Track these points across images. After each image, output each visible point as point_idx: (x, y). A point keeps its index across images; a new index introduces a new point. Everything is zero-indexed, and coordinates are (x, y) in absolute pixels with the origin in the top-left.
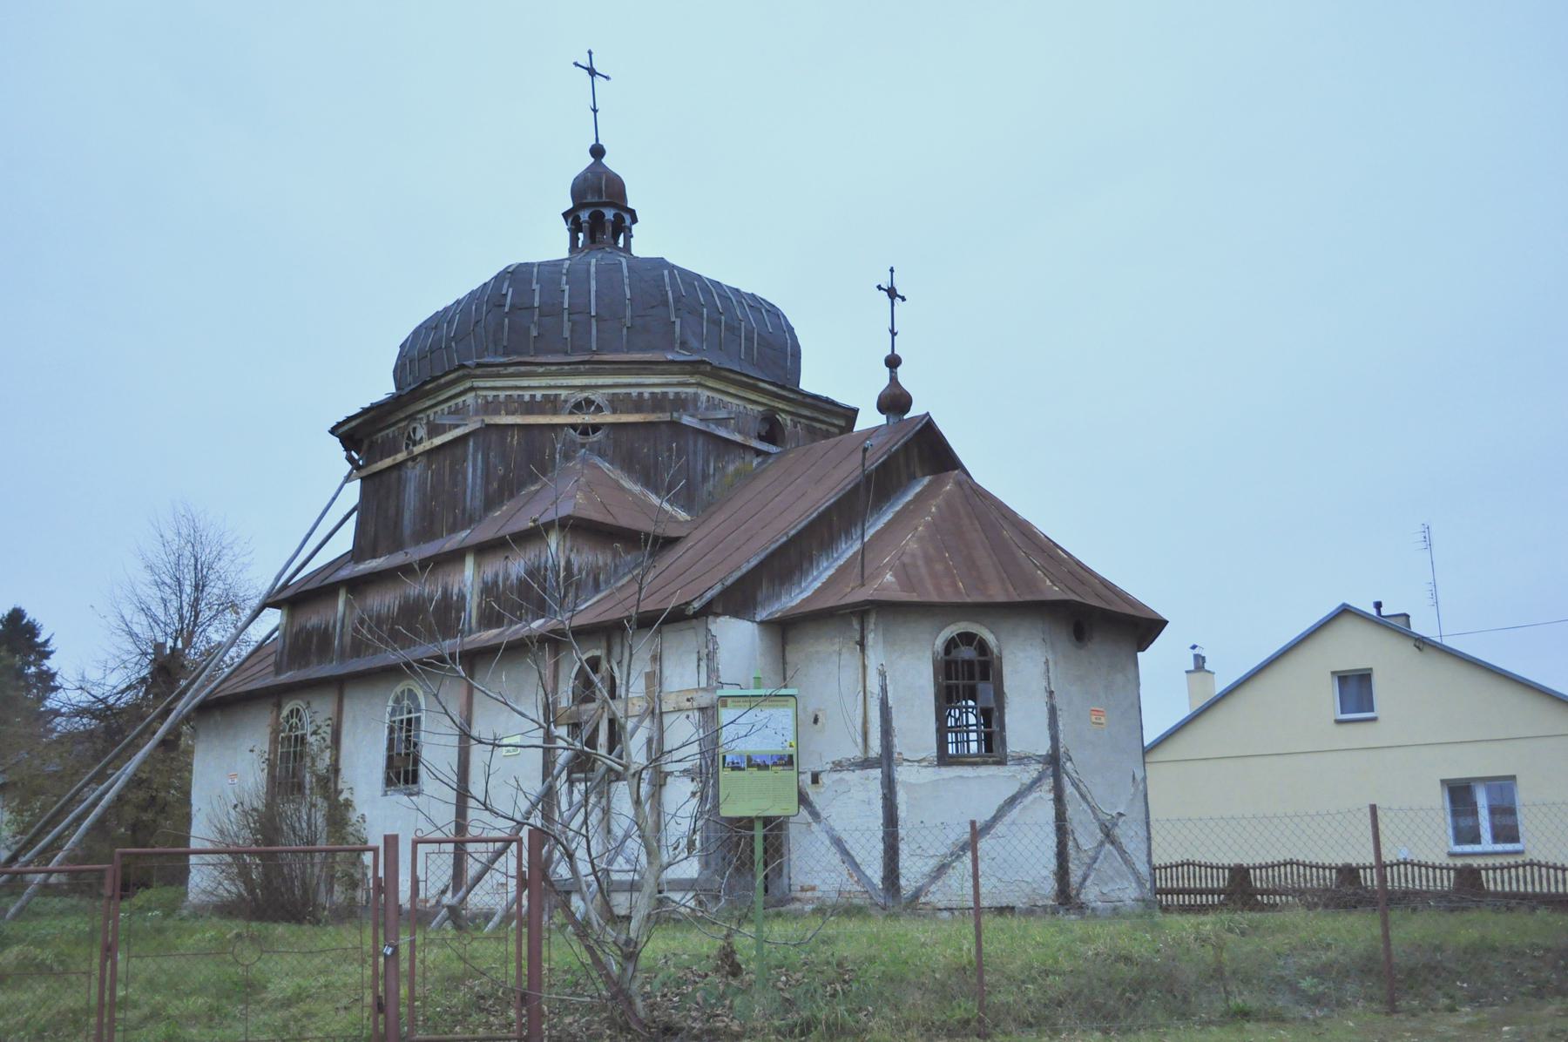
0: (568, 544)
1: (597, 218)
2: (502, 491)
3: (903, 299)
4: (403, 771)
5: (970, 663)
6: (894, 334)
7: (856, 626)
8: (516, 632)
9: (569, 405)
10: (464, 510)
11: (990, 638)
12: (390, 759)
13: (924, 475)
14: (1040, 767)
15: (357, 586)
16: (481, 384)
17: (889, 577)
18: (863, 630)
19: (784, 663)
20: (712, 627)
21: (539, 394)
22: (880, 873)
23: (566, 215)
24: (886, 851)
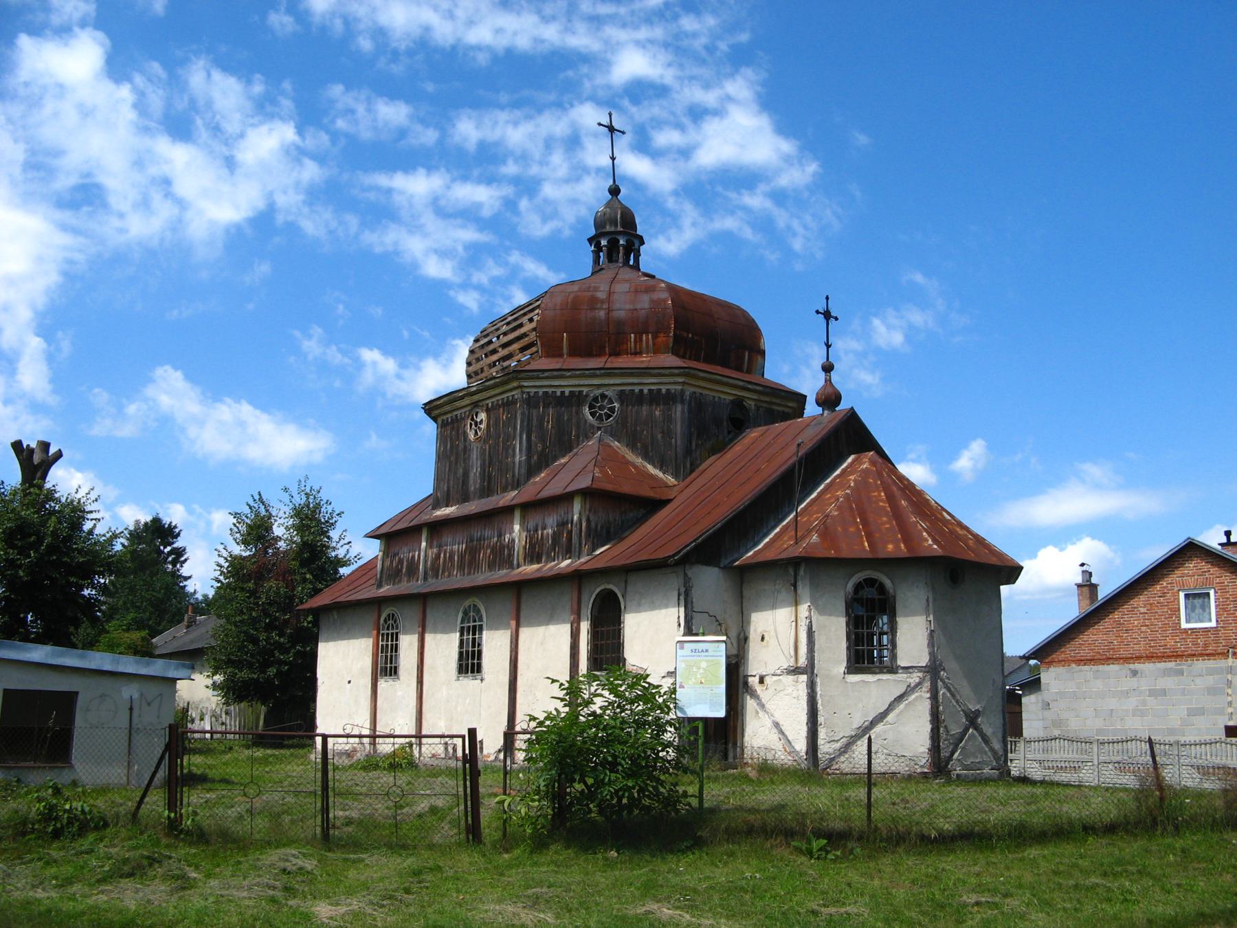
1: (613, 244)
5: (873, 600)
7: (791, 572)
9: (590, 399)
11: (888, 583)
12: (461, 654)
14: (920, 675)
15: (437, 528)
17: (815, 538)
19: (742, 593)
20: (689, 573)
21: (567, 391)
23: (590, 240)
24: (932, 730)
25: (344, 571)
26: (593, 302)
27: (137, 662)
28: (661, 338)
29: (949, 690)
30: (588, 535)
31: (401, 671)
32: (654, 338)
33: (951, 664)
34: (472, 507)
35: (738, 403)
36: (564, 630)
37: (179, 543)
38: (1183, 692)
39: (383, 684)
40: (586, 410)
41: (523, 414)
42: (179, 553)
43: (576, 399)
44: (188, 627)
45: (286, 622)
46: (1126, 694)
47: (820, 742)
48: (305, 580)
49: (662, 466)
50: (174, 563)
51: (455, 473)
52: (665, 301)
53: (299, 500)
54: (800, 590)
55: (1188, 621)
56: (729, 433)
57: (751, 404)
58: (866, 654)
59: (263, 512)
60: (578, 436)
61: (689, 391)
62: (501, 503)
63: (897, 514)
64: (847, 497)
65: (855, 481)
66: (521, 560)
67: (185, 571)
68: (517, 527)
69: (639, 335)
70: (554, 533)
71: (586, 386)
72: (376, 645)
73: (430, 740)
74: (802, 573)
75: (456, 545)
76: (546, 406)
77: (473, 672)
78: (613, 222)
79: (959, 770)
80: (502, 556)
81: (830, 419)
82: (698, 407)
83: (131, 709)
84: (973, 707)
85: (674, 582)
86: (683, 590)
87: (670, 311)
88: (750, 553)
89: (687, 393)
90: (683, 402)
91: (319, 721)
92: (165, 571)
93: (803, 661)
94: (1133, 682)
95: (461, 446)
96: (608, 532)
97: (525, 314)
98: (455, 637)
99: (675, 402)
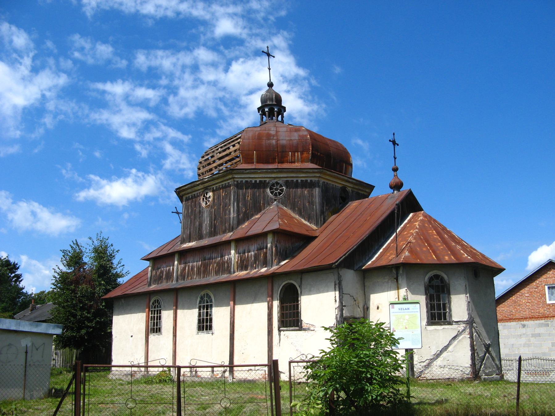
0: (276, 239)
3: (398, 145)
5: (438, 286)
6: (395, 158)
9: (270, 185)
10: (230, 224)
11: (445, 277)
12: (199, 320)
14: (464, 325)
15: (183, 254)
16: (236, 176)
17: (407, 253)
18: (397, 274)
19: (364, 283)
20: (341, 273)
21: (258, 180)
24: (472, 354)
25: (120, 280)
26: (269, 136)
27: (31, 325)
28: (305, 155)
29: (477, 333)
30: (276, 254)
31: (163, 330)
32: (302, 154)
33: (477, 320)
34: (205, 242)
35: (344, 189)
36: (263, 306)
37: (18, 272)
38: (549, 335)
39: (152, 337)
40: (268, 190)
41: (234, 192)
42: (18, 277)
43: (262, 185)
44: (32, 310)
45: (91, 306)
46: (520, 336)
47: (415, 363)
48: (100, 284)
49: (309, 219)
50: (16, 281)
51: (194, 225)
52: (306, 136)
53: (97, 243)
54: (400, 282)
55: (550, 300)
56: (340, 204)
57: (349, 189)
58: (438, 315)
59: (78, 250)
60: (264, 204)
61: (322, 181)
63: (444, 242)
64: (417, 233)
65: (419, 225)
66: (236, 269)
67: (21, 285)
68: (233, 252)
69: (294, 152)
70: (255, 254)
71: (267, 177)
72: (148, 316)
73: (240, 368)
74: (401, 272)
75: (196, 264)
76: (247, 188)
77: (206, 329)
78: (271, 100)
79: (484, 376)
80: (224, 267)
81: (398, 196)
82: (326, 190)
83: (26, 352)
84: (488, 342)
85: (332, 278)
86: (337, 282)
87: (309, 141)
88: (370, 263)
89: (321, 182)
90: (319, 187)
91: (114, 357)
92: (11, 285)
94: (523, 331)
95: (198, 210)
96: (286, 253)
97: (229, 143)
98: (196, 311)
99: (315, 187)
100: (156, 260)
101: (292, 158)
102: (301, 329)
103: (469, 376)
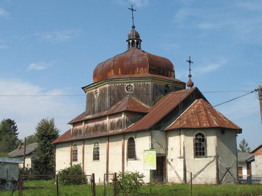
1: (133, 42)
2: (113, 103)
3: (192, 63)
4: (96, 157)
8: (117, 132)
11: (204, 134)
12: (94, 155)
13: (196, 99)
17: (185, 122)
19: (167, 137)
22: (183, 178)
23: (127, 41)
24: (217, 173)
34: (96, 115)
35: (167, 86)
44: (20, 149)
49: (146, 103)
51: (91, 107)
52: (146, 58)
57: (170, 86)
62: (103, 115)
66: (109, 130)
69: (139, 68)
83: (7, 171)
85: (149, 133)
87: (148, 61)
93: (182, 155)
95: (93, 99)
100: (75, 123)
101: (139, 71)
102: (136, 159)
103: (215, 183)
